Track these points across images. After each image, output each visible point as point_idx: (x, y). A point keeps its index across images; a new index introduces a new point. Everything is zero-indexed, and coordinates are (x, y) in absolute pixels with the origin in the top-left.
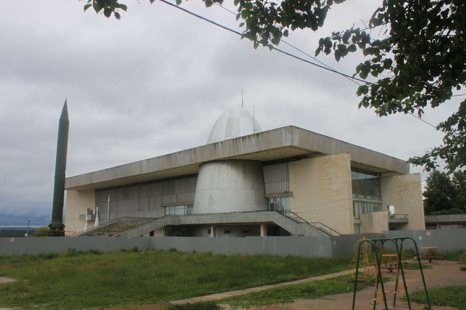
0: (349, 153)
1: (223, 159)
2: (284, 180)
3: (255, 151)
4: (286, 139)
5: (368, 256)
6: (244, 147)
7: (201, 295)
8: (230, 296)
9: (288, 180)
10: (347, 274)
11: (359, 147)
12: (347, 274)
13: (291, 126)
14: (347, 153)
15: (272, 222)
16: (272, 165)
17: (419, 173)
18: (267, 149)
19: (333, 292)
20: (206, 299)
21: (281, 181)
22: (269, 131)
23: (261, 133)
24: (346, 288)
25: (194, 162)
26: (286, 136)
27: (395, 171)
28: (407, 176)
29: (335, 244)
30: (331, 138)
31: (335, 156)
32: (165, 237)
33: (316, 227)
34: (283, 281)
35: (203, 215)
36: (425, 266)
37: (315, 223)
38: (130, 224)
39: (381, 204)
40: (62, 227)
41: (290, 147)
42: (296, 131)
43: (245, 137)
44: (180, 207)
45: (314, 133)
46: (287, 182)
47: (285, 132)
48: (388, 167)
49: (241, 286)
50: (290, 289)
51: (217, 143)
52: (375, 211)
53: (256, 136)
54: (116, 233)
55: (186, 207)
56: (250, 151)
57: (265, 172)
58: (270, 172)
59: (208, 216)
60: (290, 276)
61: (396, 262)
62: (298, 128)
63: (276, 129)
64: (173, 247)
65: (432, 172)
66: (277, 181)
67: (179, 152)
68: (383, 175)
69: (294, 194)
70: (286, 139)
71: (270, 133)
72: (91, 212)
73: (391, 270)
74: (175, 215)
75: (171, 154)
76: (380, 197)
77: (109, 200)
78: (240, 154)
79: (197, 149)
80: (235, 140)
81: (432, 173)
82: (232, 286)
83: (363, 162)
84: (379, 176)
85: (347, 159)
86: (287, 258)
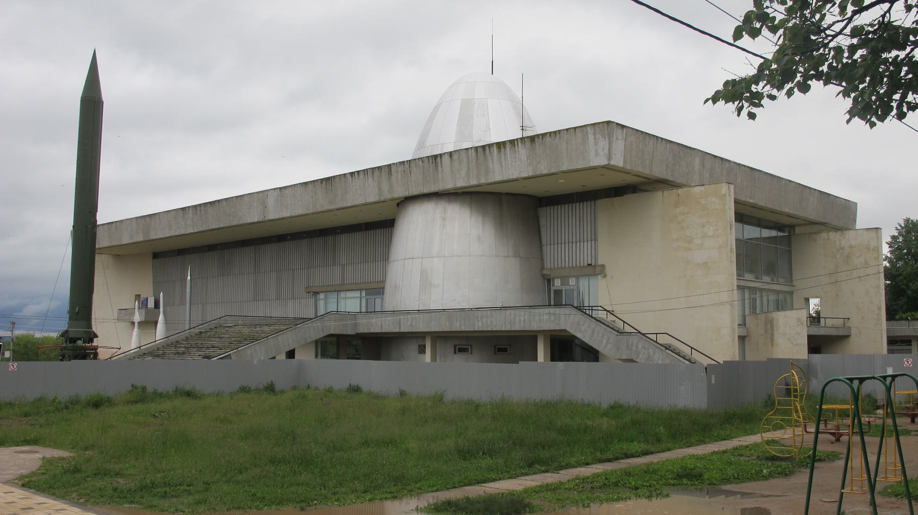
0: (732, 184)
1: (452, 191)
2: (585, 239)
3: (525, 175)
4: (597, 151)
5: (802, 409)
6: (501, 166)
7: (478, 482)
8: (534, 484)
9: (595, 239)
10: (750, 444)
11: (749, 169)
12: (751, 443)
13: (609, 123)
14: (727, 184)
15: (565, 331)
16: (559, 206)
17: (877, 229)
18: (553, 170)
19: (738, 478)
20: (490, 489)
21: (580, 242)
22: (558, 133)
23: (541, 137)
24: (762, 471)
25: (387, 196)
26: (596, 144)
27: (824, 221)
28: (851, 234)
29: (713, 382)
30: (690, 148)
31: (702, 188)
32: (316, 360)
34: (627, 456)
35: (408, 312)
36: (906, 430)
38: (246, 331)
39: (791, 293)
40: (92, 336)
41: (604, 167)
42: (618, 133)
43: (504, 143)
44: (349, 294)
45: (656, 139)
46: (593, 242)
47: (595, 134)
48: (811, 212)
49: (549, 465)
50: (649, 471)
51: (441, 155)
52: (778, 310)
53: (530, 142)
54: (219, 352)
55: (364, 294)
56: (513, 174)
57: (543, 222)
59: (421, 315)
60: (636, 446)
61: (848, 421)
62: (623, 127)
63: (575, 128)
64: (355, 382)
65: (903, 226)
66: (571, 241)
67: (352, 174)
68: (798, 230)
69: (608, 271)
70: (597, 151)
71: (560, 137)
72: (145, 302)
73: (838, 437)
74: (337, 312)
75: (334, 177)
76: (790, 280)
77: (189, 278)
78: (491, 179)
79: (393, 168)
80: (480, 150)
81: (902, 228)
82: (530, 465)
83: (757, 203)
84: (790, 232)
85: (728, 197)
86: (612, 407)
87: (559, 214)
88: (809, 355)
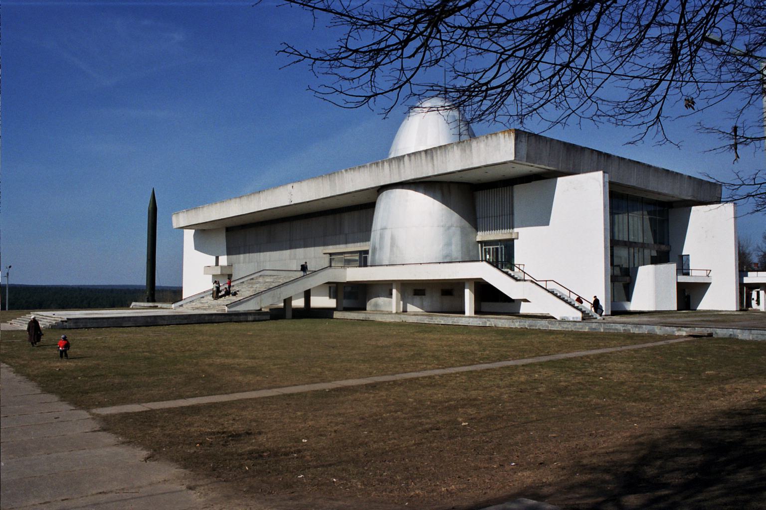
1: (412, 181)
33: (547, 288)
37: (546, 281)
46: (511, 215)
57: (516, 195)
58: (506, 192)
87: (488, 197)
88: (287, 317)
